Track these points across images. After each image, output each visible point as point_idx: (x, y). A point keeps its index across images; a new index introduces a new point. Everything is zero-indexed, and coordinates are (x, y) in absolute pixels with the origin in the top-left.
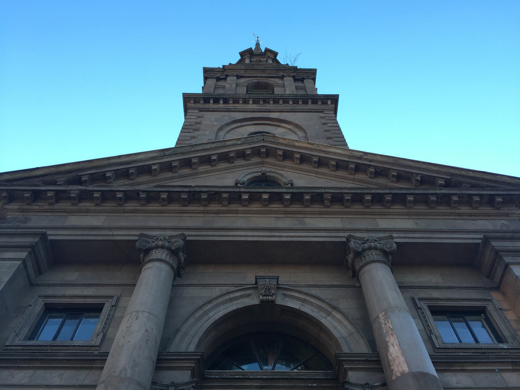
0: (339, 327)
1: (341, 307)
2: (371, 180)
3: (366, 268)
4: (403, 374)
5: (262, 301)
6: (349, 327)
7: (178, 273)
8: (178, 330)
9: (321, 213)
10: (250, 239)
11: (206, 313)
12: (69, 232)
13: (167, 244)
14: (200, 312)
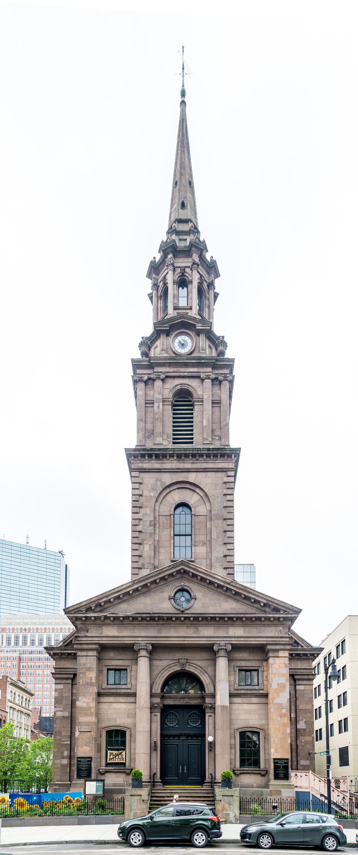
0: (205, 680)
1: (208, 672)
6: (209, 680)
7: (151, 660)
9: (206, 624)
10: (176, 642)
11: (162, 674)
13: (145, 647)
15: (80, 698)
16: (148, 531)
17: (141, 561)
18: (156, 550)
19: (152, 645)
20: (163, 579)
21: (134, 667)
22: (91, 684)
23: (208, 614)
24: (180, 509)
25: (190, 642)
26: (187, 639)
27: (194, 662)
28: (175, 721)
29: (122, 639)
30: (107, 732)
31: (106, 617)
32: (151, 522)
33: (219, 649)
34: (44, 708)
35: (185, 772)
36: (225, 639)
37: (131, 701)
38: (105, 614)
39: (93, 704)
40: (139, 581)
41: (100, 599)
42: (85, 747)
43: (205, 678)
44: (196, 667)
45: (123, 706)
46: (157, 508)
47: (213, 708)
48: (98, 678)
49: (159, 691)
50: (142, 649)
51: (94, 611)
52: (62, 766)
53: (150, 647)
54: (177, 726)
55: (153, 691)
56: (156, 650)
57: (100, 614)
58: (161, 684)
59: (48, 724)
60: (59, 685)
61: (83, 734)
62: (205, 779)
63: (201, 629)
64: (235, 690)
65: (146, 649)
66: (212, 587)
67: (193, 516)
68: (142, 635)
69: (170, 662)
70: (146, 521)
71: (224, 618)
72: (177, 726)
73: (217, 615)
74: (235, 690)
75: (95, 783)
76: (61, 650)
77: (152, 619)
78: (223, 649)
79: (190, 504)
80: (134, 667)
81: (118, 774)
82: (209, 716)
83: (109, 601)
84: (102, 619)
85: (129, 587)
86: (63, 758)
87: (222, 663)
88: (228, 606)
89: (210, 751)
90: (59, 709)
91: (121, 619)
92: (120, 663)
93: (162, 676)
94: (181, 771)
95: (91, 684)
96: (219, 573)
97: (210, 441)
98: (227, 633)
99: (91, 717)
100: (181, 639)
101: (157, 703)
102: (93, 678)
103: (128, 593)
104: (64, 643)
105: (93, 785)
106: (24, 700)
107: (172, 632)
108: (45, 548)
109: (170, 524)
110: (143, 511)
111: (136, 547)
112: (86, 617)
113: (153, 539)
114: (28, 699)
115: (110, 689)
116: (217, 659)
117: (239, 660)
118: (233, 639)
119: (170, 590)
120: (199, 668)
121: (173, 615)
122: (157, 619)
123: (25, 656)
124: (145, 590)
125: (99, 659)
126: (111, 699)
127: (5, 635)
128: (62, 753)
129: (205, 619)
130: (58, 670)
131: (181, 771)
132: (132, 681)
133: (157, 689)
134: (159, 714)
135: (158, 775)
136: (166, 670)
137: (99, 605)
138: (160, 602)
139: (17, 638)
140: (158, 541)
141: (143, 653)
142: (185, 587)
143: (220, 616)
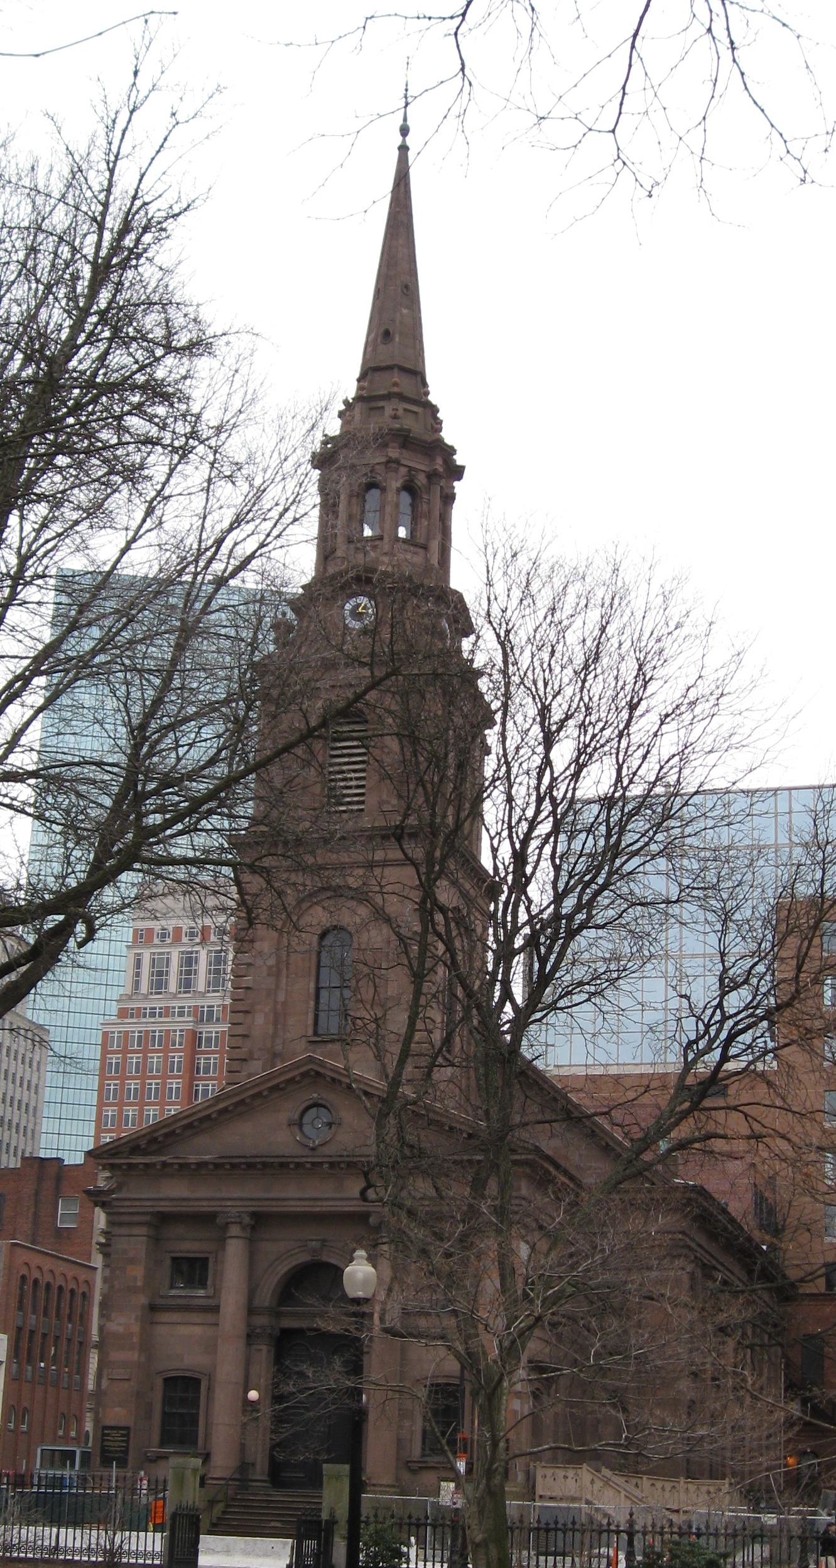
7: (252, 1243)
25: (328, 1209)
26: (319, 1203)
30: (166, 1380)
31: (165, 1164)
38: (163, 1158)
39: (136, 1328)
41: (155, 1131)
42: (116, 1409)
45: (197, 1330)
51: (145, 1153)
53: (247, 1220)
55: (257, 1303)
56: (260, 1222)
68: (235, 1196)
77: (250, 1166)
97: (394, 806)
100: (306, 1203)
112: (129, 1164)
119: (289, 1109)
126: (175, 1317)
133: (266, 1296)
137: (155, 1140)
138: (269, 1133)
140: (284, 1003)
141: (235, 1230)
142: (320, 1102)
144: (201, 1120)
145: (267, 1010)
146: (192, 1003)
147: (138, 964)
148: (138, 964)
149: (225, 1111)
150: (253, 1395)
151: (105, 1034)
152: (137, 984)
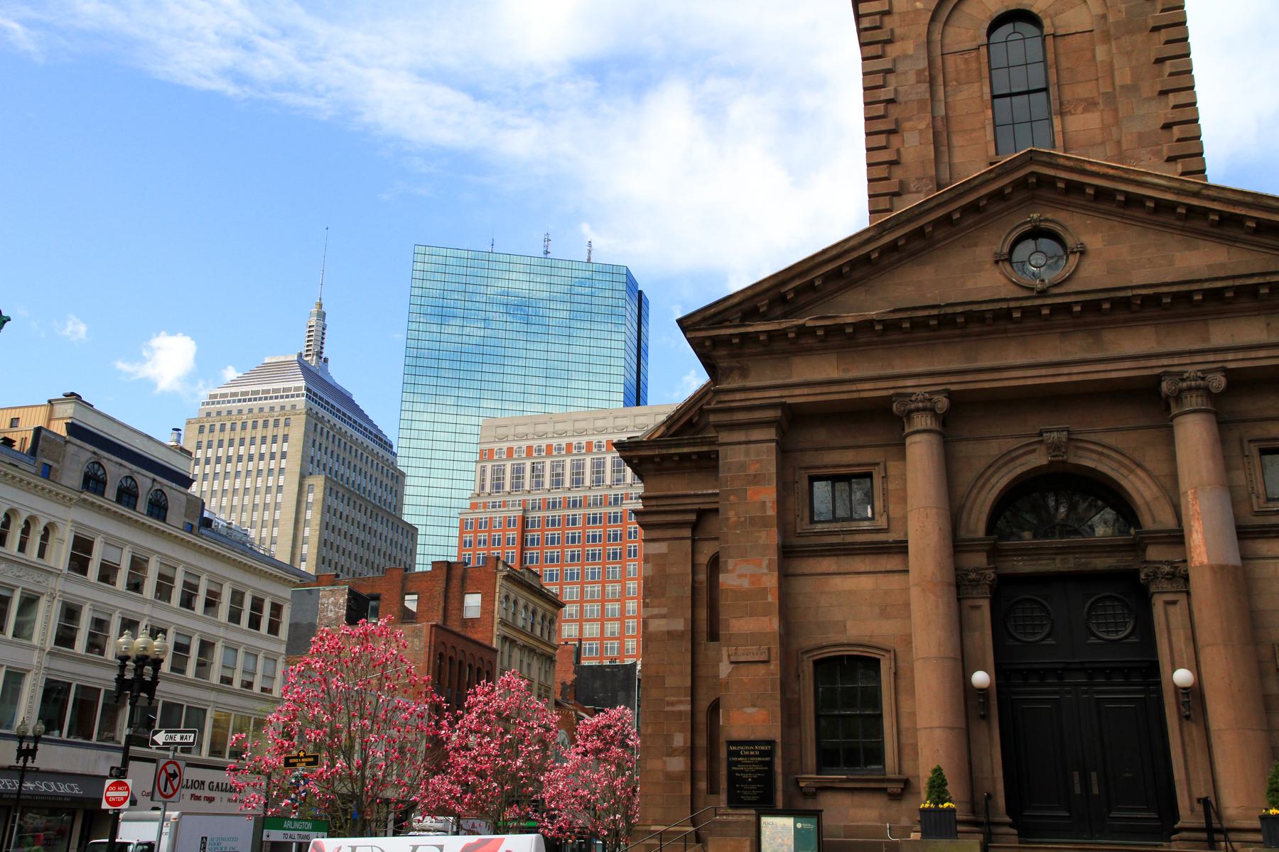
0: (1140, 488)
1: (1149, 465)
2: (1212, 230)
3: (1181, 419)
4: (1202, 565)
5: (1051, 462)
8: (964, 506)
10: (1029, 382)
11: (988, 480)
12: (806, 391)
14: (982, 481)
15: (731, 563)
16: (913, 97)
17: (898, 173)
18: (941, 138)
19: (950, 395)
20: (973, 208)
21: (893, 467)
22: (759, 522)
23: (1132, 288)
24: (1007, 29)
26: (1066, 370)
27: (1092, 437)
28: (1042, 626)
29: (854, 387)
30: (816, 663)
31: (802, 331)
32: (919, 73)
33: (1181, 391)
34: (586, 645)
35: (1096, 791)
36: (1198, 359)
37: (889, 567)
38: (801, 322)
40: (899, 222)
41: (784, 283)
42: (750, 710)
43: (1139, 484)
44: (1101, 454)
45: (866, 583)
46: (937, 37)
47: (1180, 577)
48: (781, 502)
49: (981, 532)
50: (918, 410)
51: (764, 317)
52: (669, 776)
54: (1050, 641)
56: (961, 414)
57: (785, 324)
58: (986, 510)
59: (598, 684)
60: (656, 545)
61: (744, 669)
62: (1175, 816)
63: (1108, 336)
64: (1257, 514)
65: (932, 410)
66: (1138, 214)
67: (1050, 40)
68: (917, 372)
69: (1013, 443)
70: (905, 73)
71: (1188, 295)
72: (1050, 641)
73: (1165, 289)
74: (1257, 514)
75: (789, 822)
76: (660, 447)
78: (1197, 388)
79: (1035, 10)
80: (893, 467)
81: (858, 798)
82: (1167, 603)
83: (810, 286)
84: (791, 335)
85: (868, 241)
86: (672, 753)
87: (1193, 435)
88: (1198, 261)
89: (1184, 718)
90: (656, 611)
91: (849, 330)
92: (848, 457)
93: (988, 486)
94: (1078, 790)
95: (759, 522)
96: (1153, 170)
98: (1207, 340)
99: (766, 619)
100: (1043, 372)
101: (976, 570)
102: (769, 504)
103: (866, 259)
104: (668, 428)
105: (784, 827)
106: (539, 618)
107: (1013, 355)
108: (589, 259)
109: (979, 69)
110: (893, 51)
111: (880, 140)
112: (742, 335)
113: (929, 115)
114: (549, 615)
115: (822, 533)
116: (1176, 421)
117: (1255, 420)
118: (1230, 356)
120: (1113, 454)
121: (1012, 304)
122: (960, 320)
123: (537, 514)
124: (917, 244)
125: (784, 452)
126: (827, 564)
127: (489, 466)
128: (668, 738)
129: (1125, 303)
130: (654, 502)
131: (1078, 790)
132: (891, 507)
134: (985, 604)
135: (1001, 801)
136: (999, 469)
137: (782, 299)
138: (974, 274)
139: (518, 471)
141: (922, 421)
142: (1043, 225)
143: (1174, 289)
144: (854, 264)
145: (923, 126)
146: (522, 498)
147: (483, 471)
148: (483, 471)
149: (893, 247)
150: (980, 678)
151: (462, 520)
152: (483, 487)
